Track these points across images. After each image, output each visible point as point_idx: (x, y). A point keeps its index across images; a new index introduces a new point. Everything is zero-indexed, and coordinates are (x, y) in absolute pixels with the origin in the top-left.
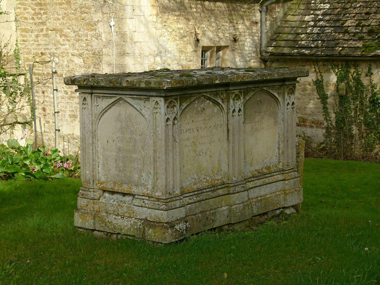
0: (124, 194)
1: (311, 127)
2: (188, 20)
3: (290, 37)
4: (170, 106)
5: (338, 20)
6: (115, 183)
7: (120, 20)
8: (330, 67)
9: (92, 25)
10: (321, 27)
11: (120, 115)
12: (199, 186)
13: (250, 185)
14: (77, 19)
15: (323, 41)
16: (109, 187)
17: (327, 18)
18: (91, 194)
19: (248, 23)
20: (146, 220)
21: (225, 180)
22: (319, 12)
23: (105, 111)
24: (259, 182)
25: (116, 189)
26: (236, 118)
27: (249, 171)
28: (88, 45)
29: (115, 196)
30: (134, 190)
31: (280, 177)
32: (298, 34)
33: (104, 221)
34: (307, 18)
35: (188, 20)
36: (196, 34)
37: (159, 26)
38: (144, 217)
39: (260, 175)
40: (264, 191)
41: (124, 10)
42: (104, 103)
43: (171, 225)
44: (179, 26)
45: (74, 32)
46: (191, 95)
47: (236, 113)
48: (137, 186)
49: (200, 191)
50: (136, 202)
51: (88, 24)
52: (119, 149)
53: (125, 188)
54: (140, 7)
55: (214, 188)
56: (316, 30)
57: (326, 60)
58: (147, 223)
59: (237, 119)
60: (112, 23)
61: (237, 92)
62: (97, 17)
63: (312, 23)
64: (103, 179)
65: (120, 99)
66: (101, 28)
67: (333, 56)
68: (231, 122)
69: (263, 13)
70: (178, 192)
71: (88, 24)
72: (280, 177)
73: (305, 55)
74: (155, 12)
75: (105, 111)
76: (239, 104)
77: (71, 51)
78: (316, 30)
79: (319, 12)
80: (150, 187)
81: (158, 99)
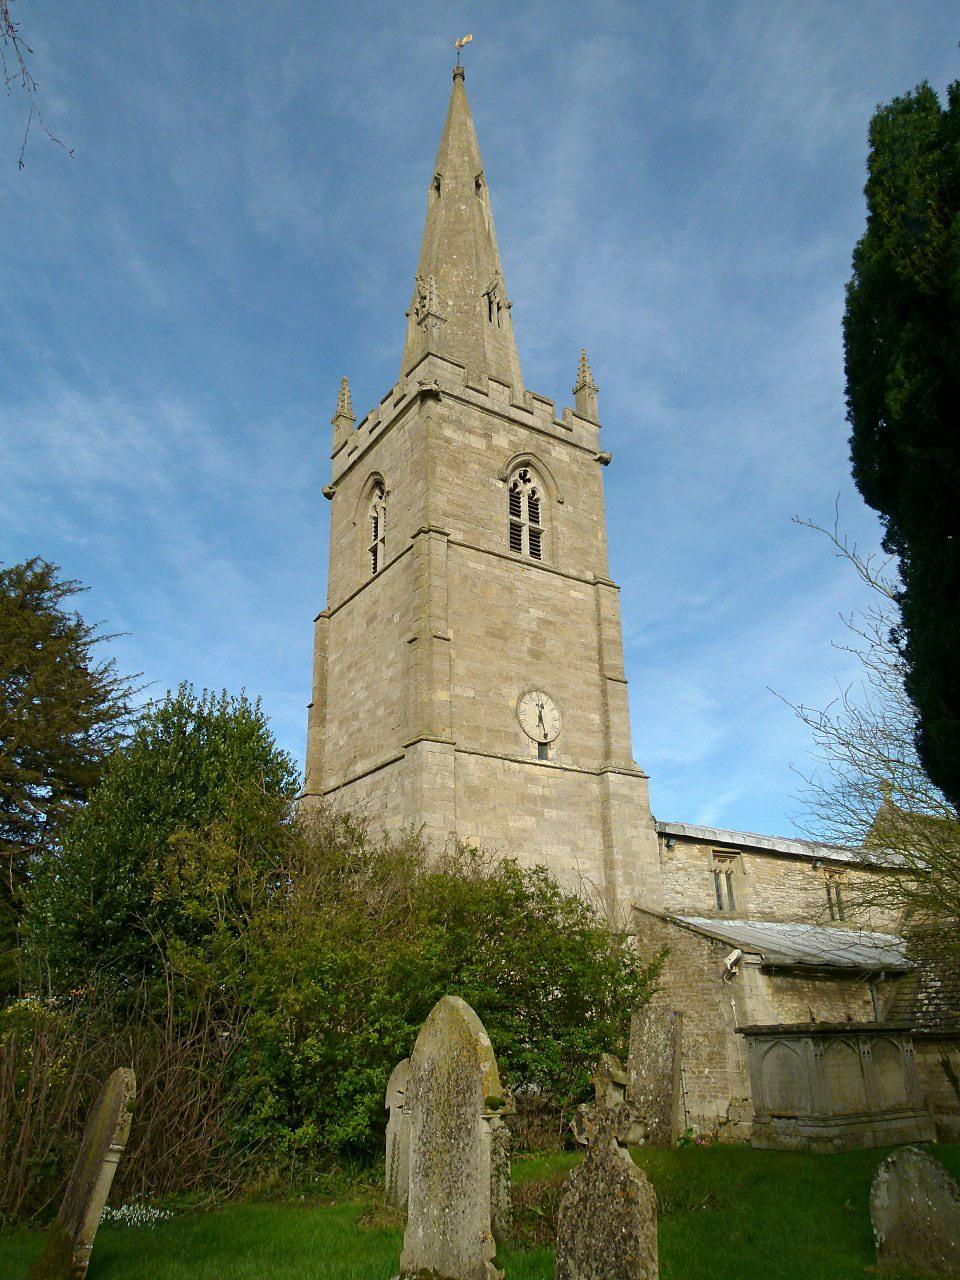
0: (789, 1118)
1: (947, 1114)
2: (802, 999)
3: (907, 1016)
4: (816, 1045)
5: (953, 998)
6: (781, 1110)
7: (740, 1000)
8: (954, 1046)
9: (714, 1006)
10: (937, 1005)
11: (779, 1055)
12: (847, 1112)
13: (887, 1117)
14: (698, 1000)
15: (941, 1019)
16: (777, 1112)
17: (941, 995)
18: (764, 1120)
19: (861, 1003)
20: (810, 1137)
21: (866, 1110)
22: (930, 990)
23: (767, 1052)
24: (893, 1116)
25: (782, 1113)
26: (867, 1059)
27: (884, 1105)
28: (711, 1025)
29: (782, 1120)
30: (797, 1114)
31: (912, 1114)
32: (915, 1013)
33: (775, 1141)
34: (920, 996)
35: (802, 999)
36: (811, 1013)
37: (776, 1005)
38: (807, 1134)
39: (894, 1110)
40: (899, 1124)
41: (469, 1132)
42: (766, 1046)
43: (830, 1140)
44: (795, 1005)
45: (698, 1013)
46: (830, 1038)
47: (866, 1055)
48: (799, 1110)
49: (847, 1116)
50: (800, 1123)
51: (710, 1005)
52: (782, 1082)
53: (789, 1113)
54: (757, 987)
55: (858, 1115)
56: (931, 1009)
57: (949, 1040)
58: (811, 1139)
59: (867, 1060)
60: (733, 1003)
61: (864, 1037)
62: (718, 998)
63: (927, 1002)
64: (771, 1107)
65: (777, 1042)
66: (722, 1008)
67: (953, 1034)
68: (864, 1060)
69: (875, 993)
70: (831, 1114)
71: (710, 1005)
72: (912, 1114)
73: (925, 1034)
74: (770, 992)
75: (767, 1052)
76: (866, 1048)
77: (695, 1031)
78: (931, 1009)
79: (930, 990)
80: (809, 1110)
81: (807, 1039)
